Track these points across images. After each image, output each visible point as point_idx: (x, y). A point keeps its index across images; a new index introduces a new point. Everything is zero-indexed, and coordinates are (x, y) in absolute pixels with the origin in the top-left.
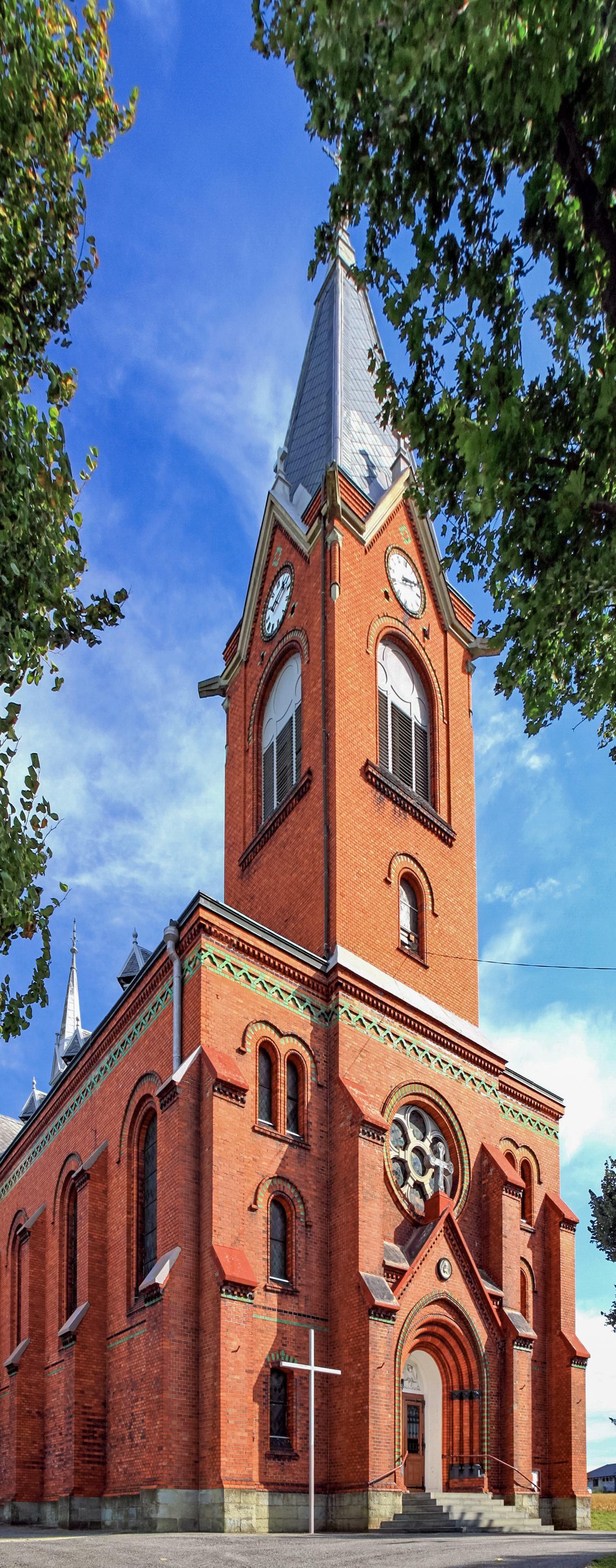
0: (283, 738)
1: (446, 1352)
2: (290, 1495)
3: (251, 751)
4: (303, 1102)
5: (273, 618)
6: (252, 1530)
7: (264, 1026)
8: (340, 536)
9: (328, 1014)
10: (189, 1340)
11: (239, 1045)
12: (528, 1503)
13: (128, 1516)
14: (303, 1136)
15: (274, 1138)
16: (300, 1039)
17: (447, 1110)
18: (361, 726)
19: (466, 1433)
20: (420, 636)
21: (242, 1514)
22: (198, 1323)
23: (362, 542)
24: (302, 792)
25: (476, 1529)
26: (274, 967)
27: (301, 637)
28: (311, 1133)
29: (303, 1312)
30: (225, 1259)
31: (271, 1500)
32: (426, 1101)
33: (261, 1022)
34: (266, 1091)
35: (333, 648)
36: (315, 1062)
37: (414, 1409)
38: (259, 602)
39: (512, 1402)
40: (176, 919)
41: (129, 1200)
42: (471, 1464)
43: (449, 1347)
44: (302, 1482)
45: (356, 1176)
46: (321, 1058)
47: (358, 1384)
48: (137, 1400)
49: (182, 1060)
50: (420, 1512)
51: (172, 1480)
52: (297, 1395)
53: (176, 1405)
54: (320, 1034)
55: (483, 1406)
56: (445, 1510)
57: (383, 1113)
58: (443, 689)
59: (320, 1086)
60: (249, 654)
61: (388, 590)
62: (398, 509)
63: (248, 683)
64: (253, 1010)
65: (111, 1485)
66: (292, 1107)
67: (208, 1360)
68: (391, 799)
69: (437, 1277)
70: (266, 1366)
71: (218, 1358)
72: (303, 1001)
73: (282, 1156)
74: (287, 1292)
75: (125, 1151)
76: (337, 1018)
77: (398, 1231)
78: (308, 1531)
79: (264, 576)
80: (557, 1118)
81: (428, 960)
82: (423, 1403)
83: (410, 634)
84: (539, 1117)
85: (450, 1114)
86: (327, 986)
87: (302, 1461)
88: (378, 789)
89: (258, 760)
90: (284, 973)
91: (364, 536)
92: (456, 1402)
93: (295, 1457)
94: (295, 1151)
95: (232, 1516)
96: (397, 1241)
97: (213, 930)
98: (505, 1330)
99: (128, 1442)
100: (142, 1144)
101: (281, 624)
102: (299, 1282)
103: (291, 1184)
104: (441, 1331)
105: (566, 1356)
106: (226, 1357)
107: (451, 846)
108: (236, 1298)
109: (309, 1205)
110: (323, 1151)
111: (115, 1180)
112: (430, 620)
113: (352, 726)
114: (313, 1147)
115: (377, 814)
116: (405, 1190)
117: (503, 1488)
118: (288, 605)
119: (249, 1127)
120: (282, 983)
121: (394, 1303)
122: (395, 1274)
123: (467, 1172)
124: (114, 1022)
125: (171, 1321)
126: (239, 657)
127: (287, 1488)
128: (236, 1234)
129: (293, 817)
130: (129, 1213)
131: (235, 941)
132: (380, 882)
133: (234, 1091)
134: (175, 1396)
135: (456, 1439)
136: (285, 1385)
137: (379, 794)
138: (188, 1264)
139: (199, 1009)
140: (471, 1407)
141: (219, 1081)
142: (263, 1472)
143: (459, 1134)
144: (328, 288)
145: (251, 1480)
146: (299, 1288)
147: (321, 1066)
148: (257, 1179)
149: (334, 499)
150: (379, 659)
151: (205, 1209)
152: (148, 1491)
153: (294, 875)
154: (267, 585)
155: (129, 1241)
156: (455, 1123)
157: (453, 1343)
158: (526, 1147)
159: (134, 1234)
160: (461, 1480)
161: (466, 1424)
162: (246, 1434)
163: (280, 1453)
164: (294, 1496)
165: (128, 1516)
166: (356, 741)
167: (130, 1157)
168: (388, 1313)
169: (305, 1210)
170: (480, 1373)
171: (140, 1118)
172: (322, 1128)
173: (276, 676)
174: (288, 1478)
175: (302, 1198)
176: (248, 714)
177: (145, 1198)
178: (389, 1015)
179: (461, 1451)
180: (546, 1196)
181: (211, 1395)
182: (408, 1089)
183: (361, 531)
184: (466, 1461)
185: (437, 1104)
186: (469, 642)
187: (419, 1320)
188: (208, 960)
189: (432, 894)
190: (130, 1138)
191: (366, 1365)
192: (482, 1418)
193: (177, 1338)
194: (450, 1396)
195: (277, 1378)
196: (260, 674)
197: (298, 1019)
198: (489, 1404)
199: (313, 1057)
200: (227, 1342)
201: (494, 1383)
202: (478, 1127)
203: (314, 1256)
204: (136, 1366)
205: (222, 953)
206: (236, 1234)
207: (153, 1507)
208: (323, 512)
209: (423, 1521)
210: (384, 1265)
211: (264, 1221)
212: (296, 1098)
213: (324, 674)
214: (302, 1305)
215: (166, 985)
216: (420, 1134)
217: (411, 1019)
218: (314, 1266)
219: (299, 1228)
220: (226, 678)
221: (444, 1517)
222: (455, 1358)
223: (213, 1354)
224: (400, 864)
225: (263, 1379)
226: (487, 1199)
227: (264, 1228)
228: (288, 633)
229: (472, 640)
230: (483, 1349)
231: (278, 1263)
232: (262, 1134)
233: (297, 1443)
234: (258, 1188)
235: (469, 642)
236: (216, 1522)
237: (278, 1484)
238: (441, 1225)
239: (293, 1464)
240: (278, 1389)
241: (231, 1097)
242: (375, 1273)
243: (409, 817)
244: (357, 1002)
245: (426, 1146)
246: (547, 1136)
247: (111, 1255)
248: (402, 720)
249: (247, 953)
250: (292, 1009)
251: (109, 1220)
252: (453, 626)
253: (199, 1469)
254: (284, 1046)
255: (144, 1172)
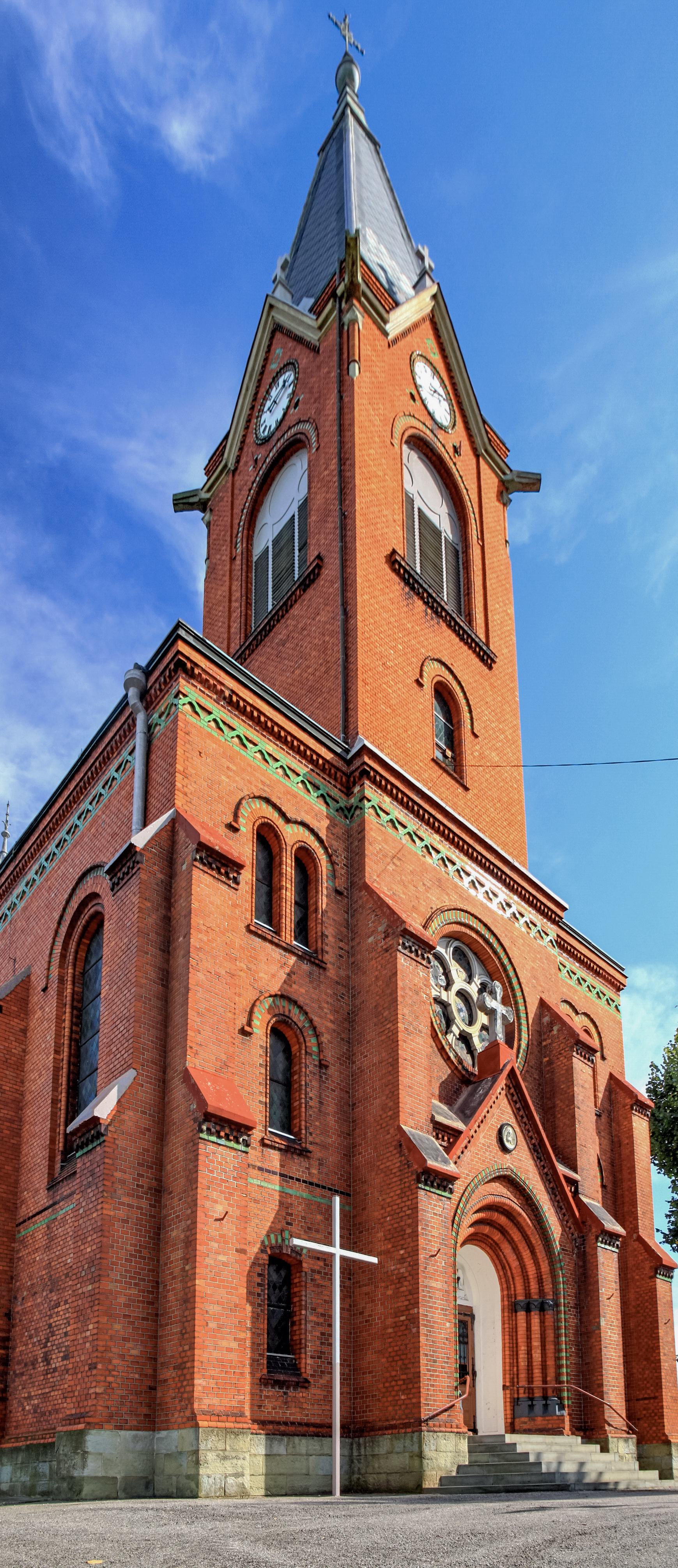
0: (282, 541)
1: (507, 1249)
2: (296, 1439)
3: (239, 558)
4: (316, 910)
5: (270, 420)
6: (243, 1493)
7: (264, 805)
8: (359, 317)
9: (349, 810)
10: (144, 1204)
11: (229, 819)
12: (624, 1448)
13: (36, 1475)
14: (316, 952)
15: (277, 945)
16: (312, 831)
17: (499, 949)
18: (385, 512)
19: (537, 1355)
20: (451, 451)
21: (228, 1467)
22: (159, 1180)
23: (385, 334)
24: (309, 580)
25: (557, 1486)
26: (278, 737)
27: (307, 427)
28: (327, 948)
29: (315, 1181)
30: (207, 1088)
31: (269, 1446)
32: (474, 935)
33: (260, 797)
34: (265, 888)
35: (352, 424)
36: (332, 863)
37: (465, 1322)
38: (252, 408)
39: (598, 1316)
40: (143, 663)
41: (58, 1035)
42: (545, 1397)
43: (511, 1242)
44: (317, 1420)
45: (394, 1001)
46: (340, 859)
47: (401, 1279)
48: (58, 1305)
49: (145, 824)
50: (495, 1461)
51: (111, 1416)
52: (308, 1296)
53: (122, 1300)
54: (338, 831)
55: (558, 1320)
56: (532, 1459)
57: (425, 927)
58: (476, 506)
59: (338, 892)
60: (238, 461)
61: (414, 392)
62: (424, 319)
63: (236, 492)
64: (250, 783)
65: (12, 1431)
66: (300, 915)
67: (176, 1233)
68: (422, 598)
69: (491, 1151)
70: (263, 1251)
71: (192, 1229)
72: (316, 787)
73: (287, 970)
74: (294, 1150)
75: (55, 972)
76: (363, 814)
77: (443, 1085)
78: (330, 1493)
79: (259, 381)
80: (619, 989)
81: (471, 774)
82: (473, 1317)
83: (439, 445)
84: (600, 985)
85: (502, 955)
86: (348, 776)
87: (315, 1391)
88: (407, 583)
89: (249, 567)
90: (292, 748)
91: (388, 327)
92: (521, 1315)
93: (304, 1384)
94: (306, 967)
95: (212, 1471)
96: (442, 1099)
97: (197, 671)
98: (584, 1223)
99: (41, 1367)
100: (80, 964)
101: (280, 424)
102: (310, 1139)
103: (300, 1008)
104: (503, 1220)
105: (647, 1265)
106: (206, 1228)
107: (490, 668)
108: (223, 1141)
109: (325, 1038)
110: (343, 973)
111: (39, 1014)
112: (458, 436)
113: (376, 509)
114: (329, 966)
115: (405, 609)
116: (450, 1037)
117: (590, 1428)
118: (290, 401)
119: (242, 927)
120: (287, 759)
121: (450, 1168)
122: (449, 1136)
123: (524, 1028)
124: (48, 819)
125: (118, 1175)
126: (226, 466)
127: (292, 1429)
128: (224, 1057)
129: (296, 611)
130: (57, 1052)
131: (227, 693)
132: (410, 681)
133: (223, 865)
134: (121, 1287)
135: (523, 1363)
136: (288, 1282)
137: (407, 589)
138: (147, 1093)
139: (173, 765)
140: (542, 1322)
141: (202, 847)
142: (257, 1405)
143: (514, 981)
144: (335, 135)
145: (242, 1415)
146: (310, 1147)
147: (341, 871)
148: (252, 995)
149: (353, 275)
150: (405, 461)
151: (177, 1018)
152: (70, 1433)
153: (297, 672)
154: (262, 391)
155: (55, 1089)
156: (509, 967)
157: (516, 1236)
158: (585, 1014)
159: (64, 1080)
160: (533, 1419)
161: (536, 1343)
162: (234, 1345)
163: (282, 1377)
164: (304, 1441)
165: (36, 1475)
166: (378, 532)
167: (61, 980)
168: (444, 1182)
169: (319, 1044)
170: (554, 1276)
171: (79, 929)
172: (341, 944)
173: (273, 479)
174: (293, 1414)
175: (315, 1028)
176: (236, 521)
177: (81, 1033)
178: (428, 823)
179: (530, 1379)
180: (611, 1075)
181: (179, 1286)
182: (453, 916)
183: (385, 322)
184: (538, 1394)
185: (487, 941)
186: (504, 473)
187: (476, 1201)
188: (188, 707)
189: (470, 711)
190: (63, 956)
191: (414, 1252)
192: (557, 1336)
193: (126, 1200)
194: (511, 1307)
195: (277, 1271)
196: (252, 479)
197: (307, 810)
198: (567, 1319)
199: (330, 856)
200: (208, 1204)
201: (571, 1291)
202: (535, 978)
203: (331, 1108)
204: (59, 1257)
205: (209, 704)
206: (224, 1057)
207: (78, 1459)
208: (339, 292)
209: (497, 1477)
210: (433, 1120)
211: (261, 1052)
212: (304, 904)
213: (340, 452)
214: (315, 1171)
215: (125, 754)
216: (464, 975)
217: (455, 834)
218: (331, 1121)
219: (311, 1068)
220: (209, 490)
221: (534, 1470)
222: (520, 1258)
223: (183, 1225)
224: (433, 671)
225: (259, 1270)
226: (550, 1063)
227: (261, 1061)
228: (290, 428)
229: (508, 472)
230: (557, 1246)
231: (279, 1113)
232: (260, 936)
233: (308, 1364)
234: (254, 1005)
235: (504, 473)
236: (183, 1481)
237: (278, 1423)
238: (502, 1081)
239: (301, 1394)
240: (281, 1280)
241: (220, 873)
242: (421, 1129)
243: (444, 625)
244: (387, 799)
245: (473, 990)
246: (607, 1007)
247: (29, 1112)
248: (429, 530)
249: (243, 712)
250: (302, 793)
251: (28, 1066)
252: (486, 451)
253: (157, 1397)
254: (291, 835)
255: (81, 1001)
